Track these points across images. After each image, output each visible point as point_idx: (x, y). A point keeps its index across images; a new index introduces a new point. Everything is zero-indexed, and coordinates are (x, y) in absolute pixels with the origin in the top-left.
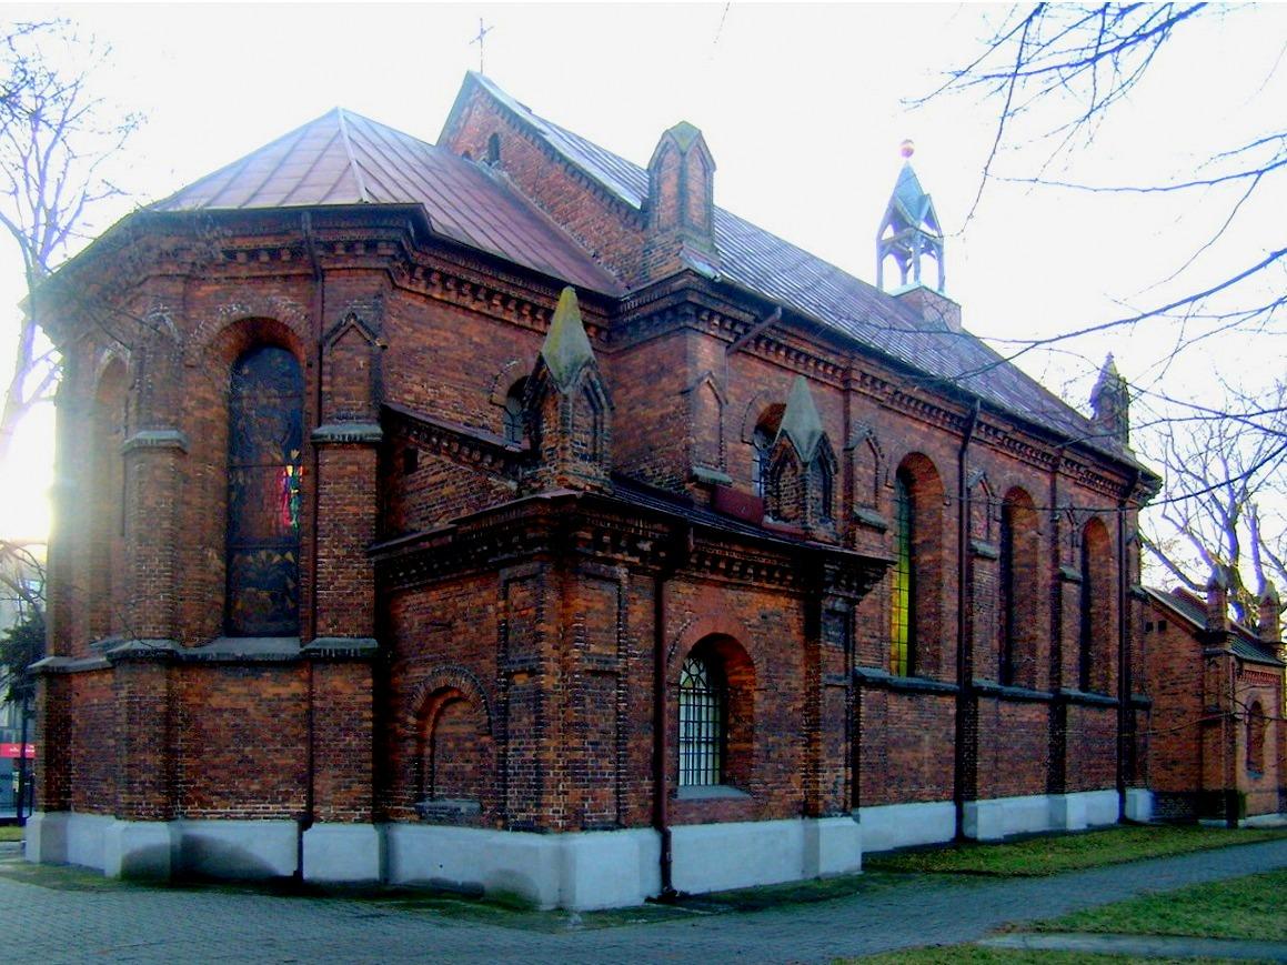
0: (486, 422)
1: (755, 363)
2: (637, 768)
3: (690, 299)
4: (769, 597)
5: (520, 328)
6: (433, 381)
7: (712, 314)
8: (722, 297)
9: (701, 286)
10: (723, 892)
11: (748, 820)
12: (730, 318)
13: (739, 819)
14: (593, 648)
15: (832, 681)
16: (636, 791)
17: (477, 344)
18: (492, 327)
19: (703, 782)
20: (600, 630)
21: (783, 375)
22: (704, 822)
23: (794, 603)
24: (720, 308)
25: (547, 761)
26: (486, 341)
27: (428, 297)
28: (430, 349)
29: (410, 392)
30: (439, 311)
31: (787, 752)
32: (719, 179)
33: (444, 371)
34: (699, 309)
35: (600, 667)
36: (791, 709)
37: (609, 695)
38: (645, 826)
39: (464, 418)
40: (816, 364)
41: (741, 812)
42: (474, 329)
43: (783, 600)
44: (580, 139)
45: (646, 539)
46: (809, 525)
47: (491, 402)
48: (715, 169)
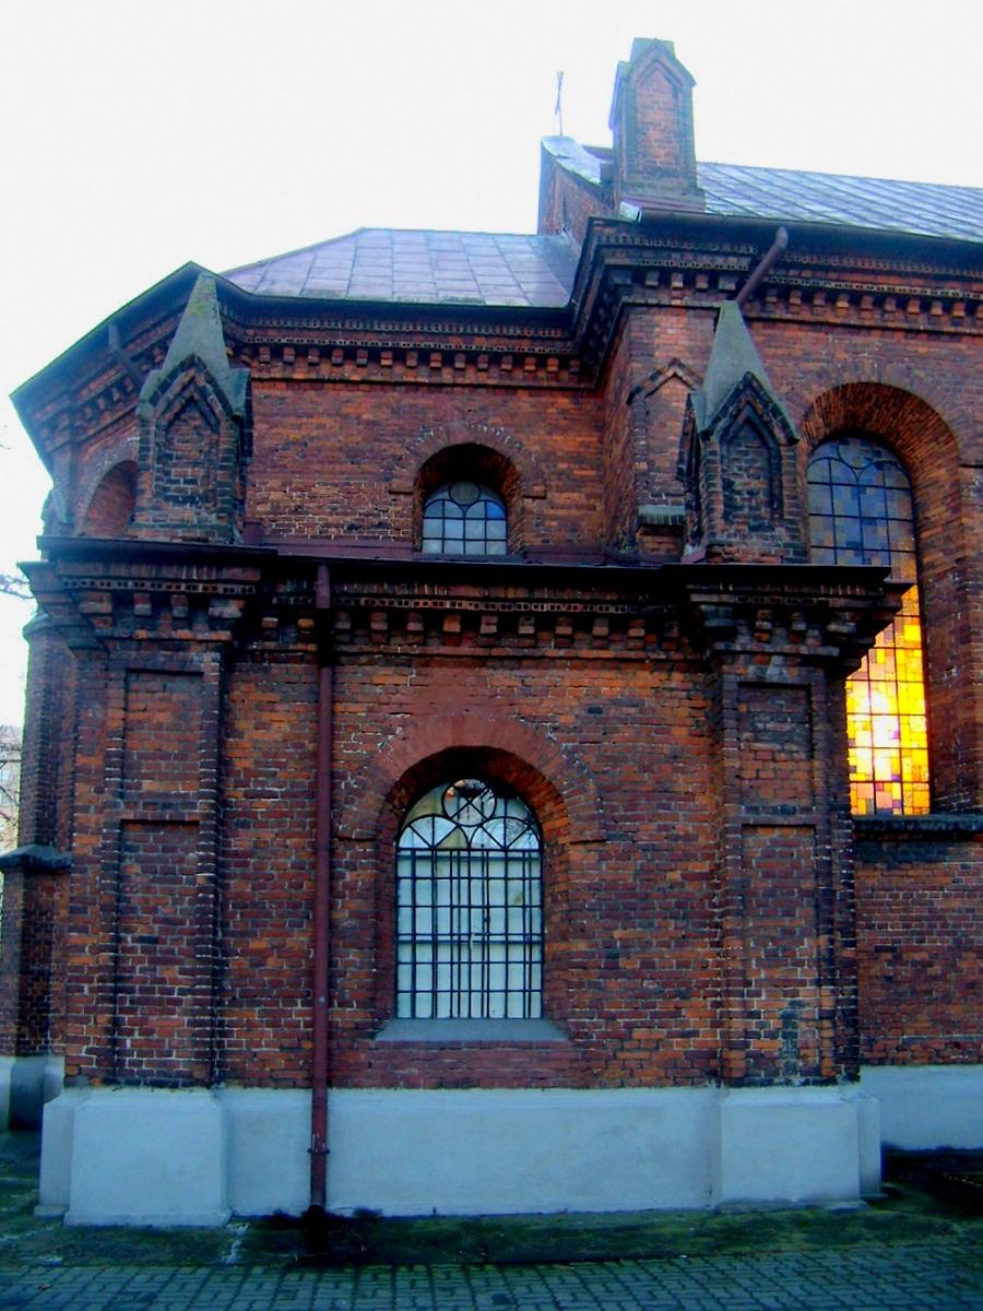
0: (383, 518)
1: (793, 332)
2: (276, 984)
3: (611, 261)
4: (606, 674)
5: (438, 387)
6: (297, 480)
7: (665, 277)
8: (677, 244)
9: (623, 237)
10: (526, 1215)
11: (563, 1085)
12: (701, 271)
13: (541, 1082)
14: (147, 785)
15: (764, 817)
16: (275, 1024)
17: (369, 423)
18: (393, 396)
19: (464, 1014)
20: (165, 757)
21: (858, 339)
22: (441, 1084)
23: (677, 678)
24: (675, 260)
25: (79, 969)
26: (383, 415)
27: (289, 381)
28: (295, 443)
29: (264, 501)
30: (310, 394)
31: (667, 959)
32: (701, 100)
33: (317, 467)
34: (638, 275)
35: (150, 815)
36: (676, 876)
37: (181, 860)
38: (295, 1086)
39: (348, 519)
40: (947, 309)
41: (542, 1070)
42: (366, 406)
43: (645, 678)
44: (890, 182)
45: (226, 597)
46: (721, 538)
47: (391, 492)
48: (692, 83)
